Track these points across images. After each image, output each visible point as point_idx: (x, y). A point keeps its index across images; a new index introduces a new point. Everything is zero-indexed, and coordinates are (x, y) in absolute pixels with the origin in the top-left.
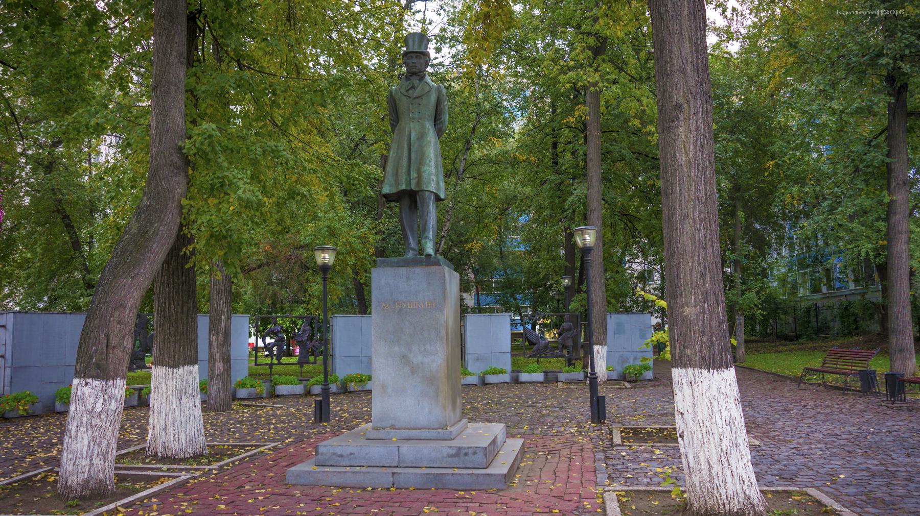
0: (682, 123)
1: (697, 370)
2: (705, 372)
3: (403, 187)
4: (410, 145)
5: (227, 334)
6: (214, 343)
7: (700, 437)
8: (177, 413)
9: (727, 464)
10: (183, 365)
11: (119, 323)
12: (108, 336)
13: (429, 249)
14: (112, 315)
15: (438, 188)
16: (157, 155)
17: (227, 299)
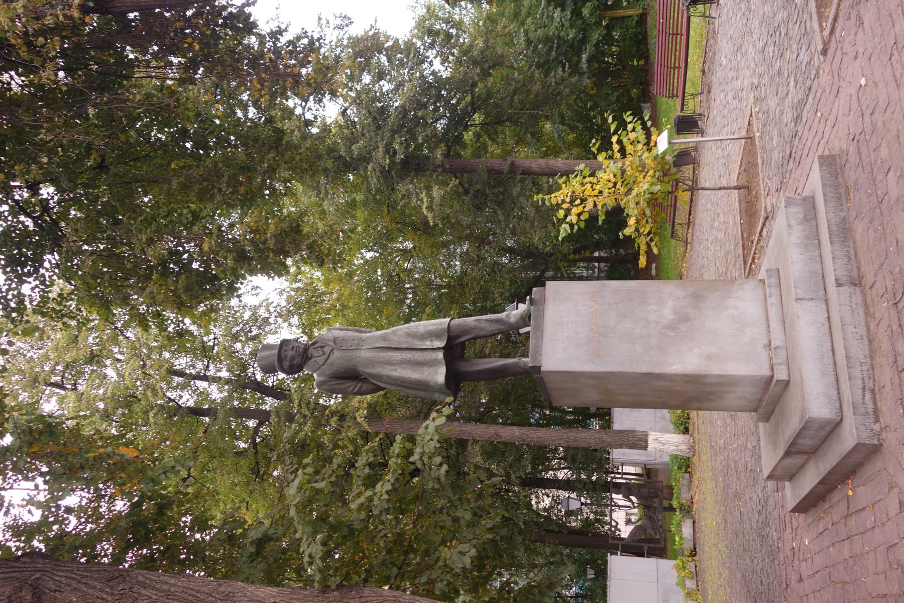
3: (440, 355)
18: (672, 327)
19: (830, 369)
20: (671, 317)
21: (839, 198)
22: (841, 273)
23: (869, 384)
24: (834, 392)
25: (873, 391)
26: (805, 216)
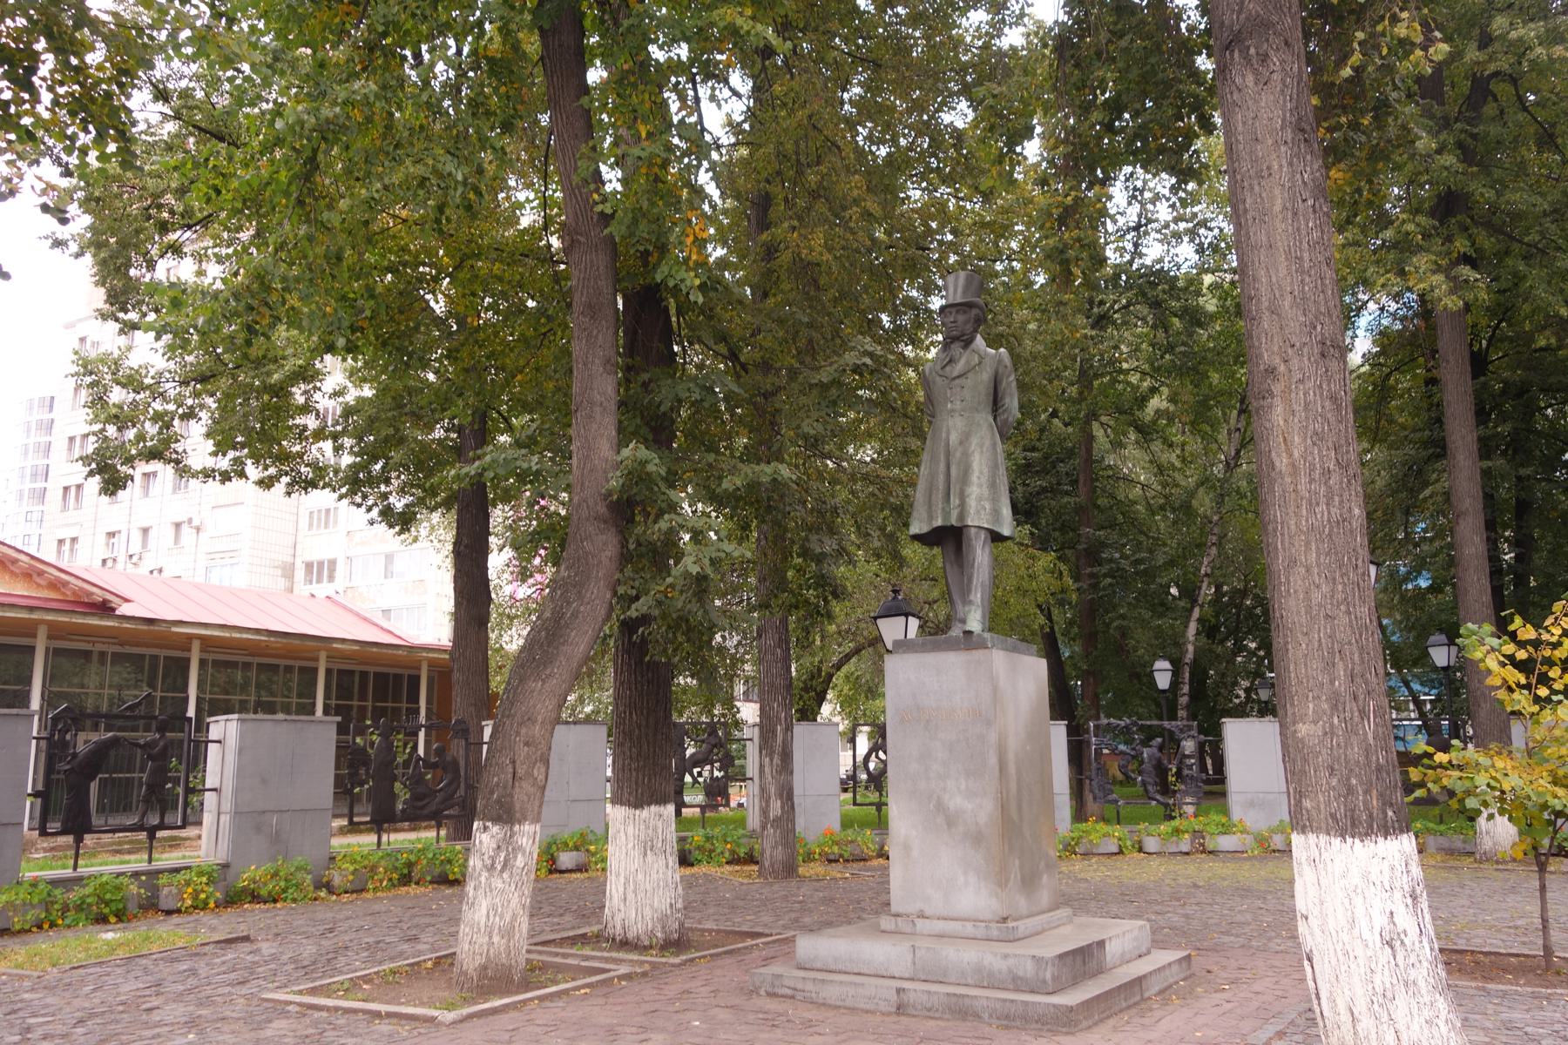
0: (1277, 401)
1: (1323, 838)
2: (1337, 841)
3: (939, 522)
4: (948, 454)
5: (787, 756)
6: (767, 770)
7: (1334, 962)
8: (640, 876)
9: (1385, 1018)
10: (649, 804)
11: (527, 744)
12: (513, 762)
13: (975, 623)
14: (518, 734)
15: (996, 513)
16: (579, 505)
17: (784, 699)
18: (940, 807)
19: (840, 967)
20: (952, 806)
21: (1007, 1017)
22: (912, 995)
23: (799, 996)
24: (819, 965)
25: (793, 997)
26: (1021, 978)
